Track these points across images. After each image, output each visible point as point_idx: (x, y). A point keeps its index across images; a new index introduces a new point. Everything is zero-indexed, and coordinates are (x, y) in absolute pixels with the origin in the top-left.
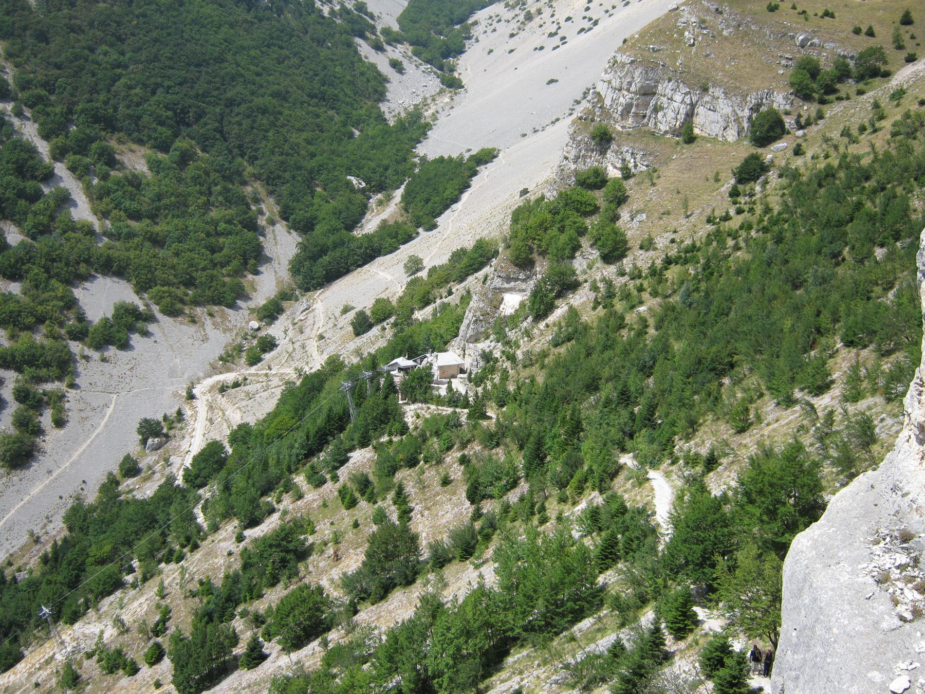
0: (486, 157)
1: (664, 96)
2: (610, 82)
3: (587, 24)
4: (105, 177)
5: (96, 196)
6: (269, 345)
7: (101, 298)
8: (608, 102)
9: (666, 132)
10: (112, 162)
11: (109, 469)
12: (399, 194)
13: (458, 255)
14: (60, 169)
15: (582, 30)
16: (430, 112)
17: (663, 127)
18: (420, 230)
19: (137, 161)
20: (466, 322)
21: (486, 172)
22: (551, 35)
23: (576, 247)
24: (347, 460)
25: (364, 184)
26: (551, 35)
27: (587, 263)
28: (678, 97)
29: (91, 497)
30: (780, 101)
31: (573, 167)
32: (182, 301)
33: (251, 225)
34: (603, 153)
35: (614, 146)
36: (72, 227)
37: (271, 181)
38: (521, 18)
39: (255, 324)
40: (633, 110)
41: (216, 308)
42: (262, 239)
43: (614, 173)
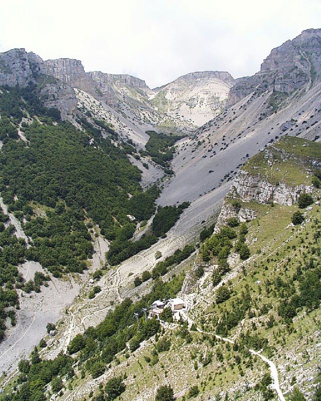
0: (186, 205)
1: (261, 187)
2: (239, 182)
3: (224, 147)
4: (29, 220)
5: (26, 228)
6: (97, 290)
7: (29, 270)
8: (238, 191)
9: (263, 202)
10: (31, 213)
11: (35, 344)
12: (150, 222)
13: (178, 251)
14: (12, 216)
15: (222, 149)
16: (160, 185)
17: (262, 200)
18: (160, 238)
19: (41, 212)
20: (184, 285)
21: (186, 211)
22: (209, 151)
23: (228, 253)
24: (139, 346)
25: (135, 218)
26: (209, 151)
27: (233, 260)
28: (267, 188)
29: (28, 358)
30: (309, 189)
31: (226, 218)
32: (61, 271)
33: (89, 239)
34: (237, 212)
35: (242, 209)
36: (15, 241)
37: (97, 219)
38: (196, 144)
39: (92, 280)
40: (249, 194)
41: (75, 274)
42: (93, 243)
43: (242, 220)
